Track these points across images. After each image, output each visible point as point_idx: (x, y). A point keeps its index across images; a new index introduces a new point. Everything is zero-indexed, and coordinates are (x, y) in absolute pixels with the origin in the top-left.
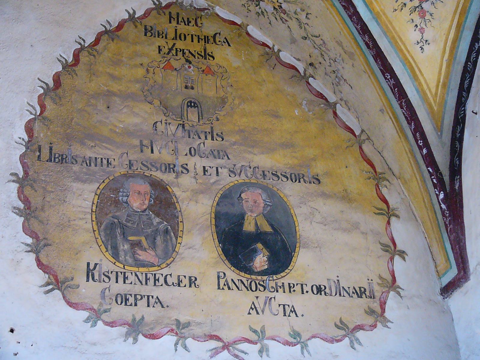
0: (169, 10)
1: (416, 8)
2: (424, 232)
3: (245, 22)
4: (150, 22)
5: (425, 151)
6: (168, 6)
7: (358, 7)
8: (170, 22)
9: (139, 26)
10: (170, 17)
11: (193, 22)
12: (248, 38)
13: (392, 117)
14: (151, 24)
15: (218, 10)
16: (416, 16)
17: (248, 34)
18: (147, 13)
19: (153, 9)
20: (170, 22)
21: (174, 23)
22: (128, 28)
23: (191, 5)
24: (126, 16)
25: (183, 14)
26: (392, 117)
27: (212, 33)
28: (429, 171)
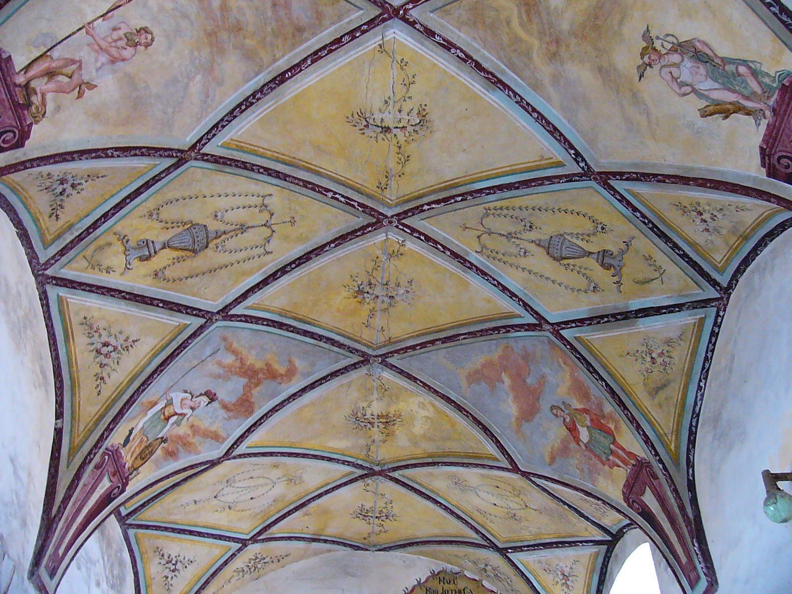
0: (439, 576)
1: (563, 584)
2: (507, 441)
3: (481, 579)
4: (429, 585)
5: (422, 238)
6: (439, 573)
7: (119, 143)
8: (440, 583)
9: (423, 588)
10: (440, 580)
11: (452, 582)
12: (483, 588)
13: (683, 233)
14: (429, 586)
15: (466, 573)
16: (564, 587)
17: (483, 585)
18: (426, 581)
19: (430, 576)
20: (440, 583)
21: (442, 584)
22: (418, 590)
23: (451, 571)
24: (416, 583)
25: (447, 577)
26: (683, 233)
27: (463, 588)
28: (415, 237)
